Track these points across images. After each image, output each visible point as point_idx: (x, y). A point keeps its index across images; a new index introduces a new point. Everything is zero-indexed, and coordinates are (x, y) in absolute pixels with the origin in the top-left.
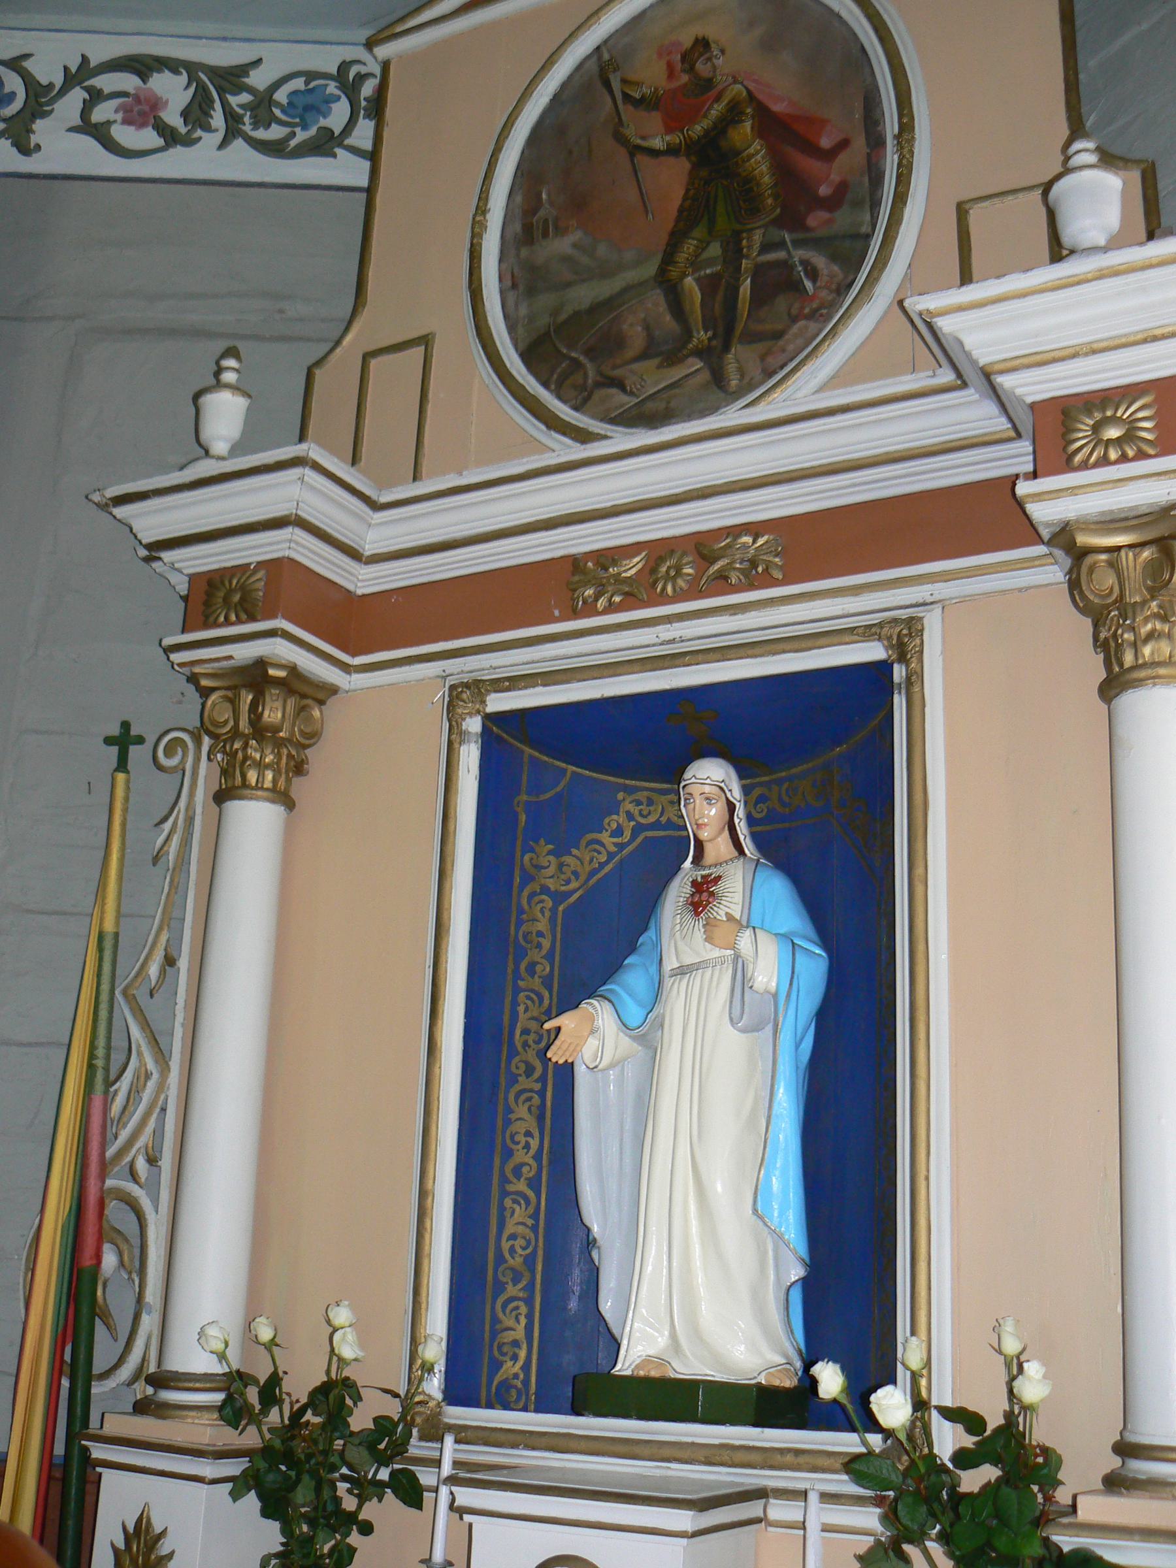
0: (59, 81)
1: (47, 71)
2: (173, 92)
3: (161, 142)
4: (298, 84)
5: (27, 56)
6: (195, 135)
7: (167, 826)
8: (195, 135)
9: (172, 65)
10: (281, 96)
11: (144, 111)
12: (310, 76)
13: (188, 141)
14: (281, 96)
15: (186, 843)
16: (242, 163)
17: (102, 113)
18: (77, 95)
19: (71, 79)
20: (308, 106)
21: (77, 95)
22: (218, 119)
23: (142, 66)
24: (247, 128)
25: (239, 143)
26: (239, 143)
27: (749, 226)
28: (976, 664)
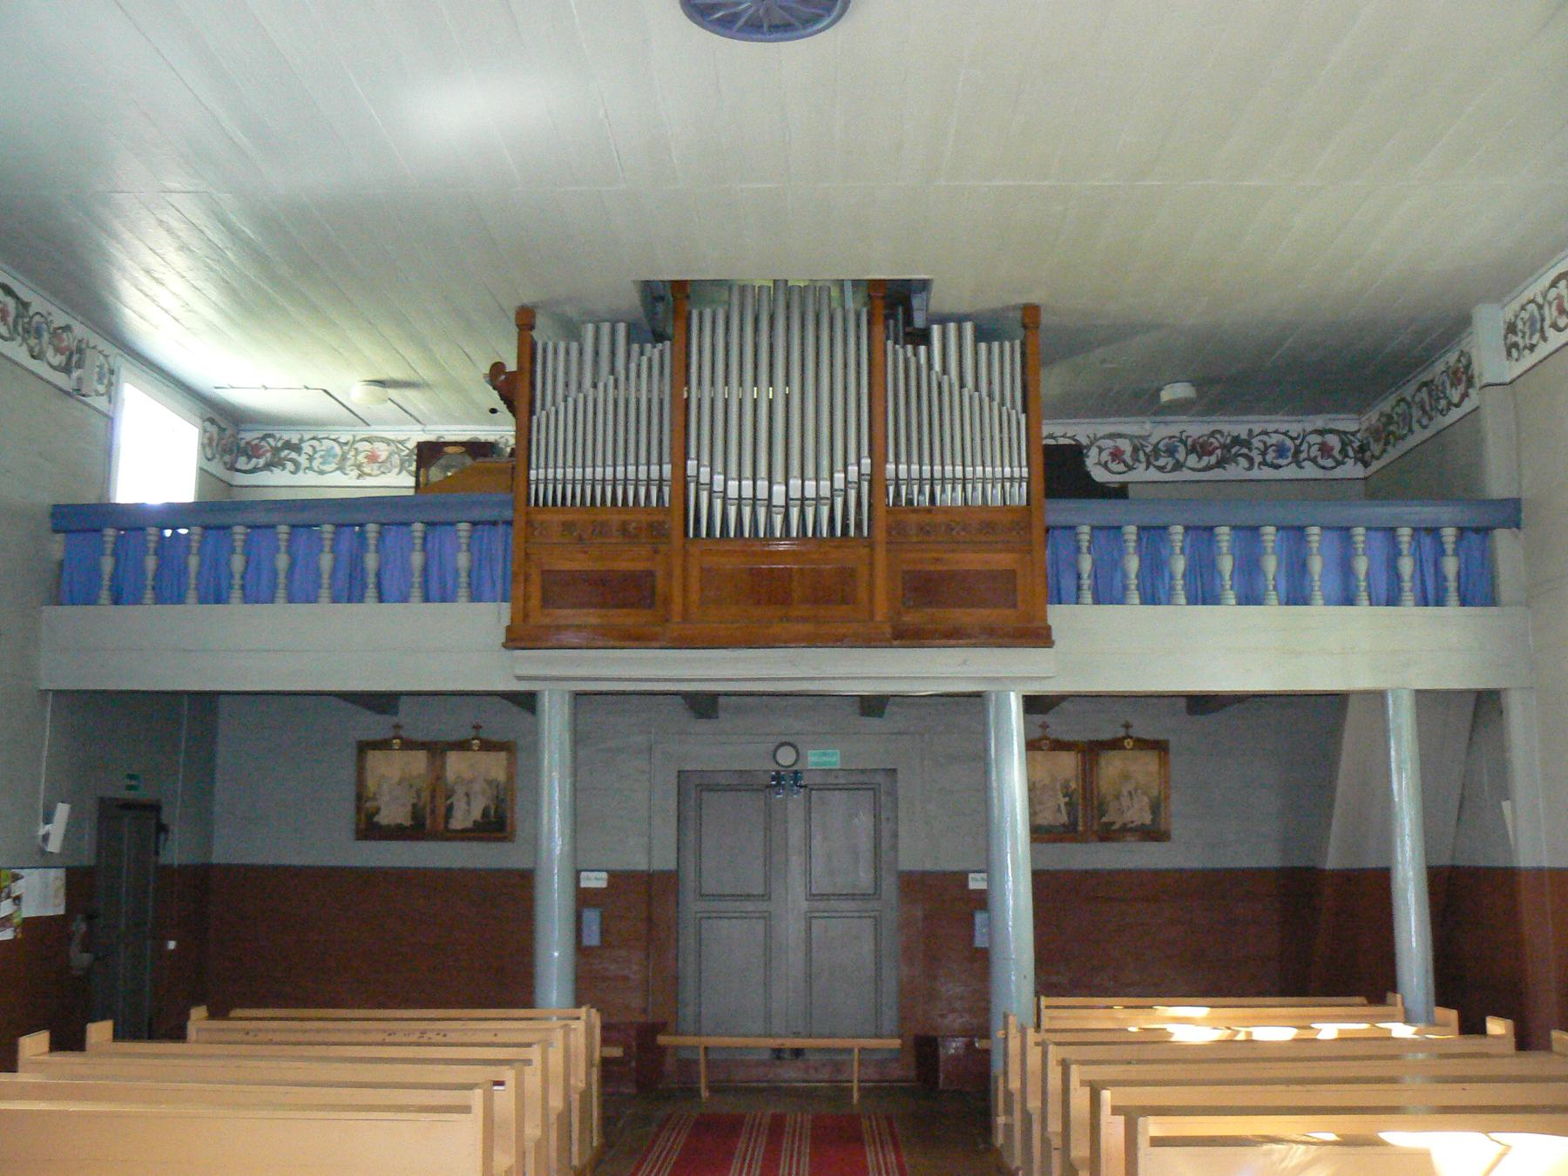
22: (1142, 457)
23: (1321, 432)
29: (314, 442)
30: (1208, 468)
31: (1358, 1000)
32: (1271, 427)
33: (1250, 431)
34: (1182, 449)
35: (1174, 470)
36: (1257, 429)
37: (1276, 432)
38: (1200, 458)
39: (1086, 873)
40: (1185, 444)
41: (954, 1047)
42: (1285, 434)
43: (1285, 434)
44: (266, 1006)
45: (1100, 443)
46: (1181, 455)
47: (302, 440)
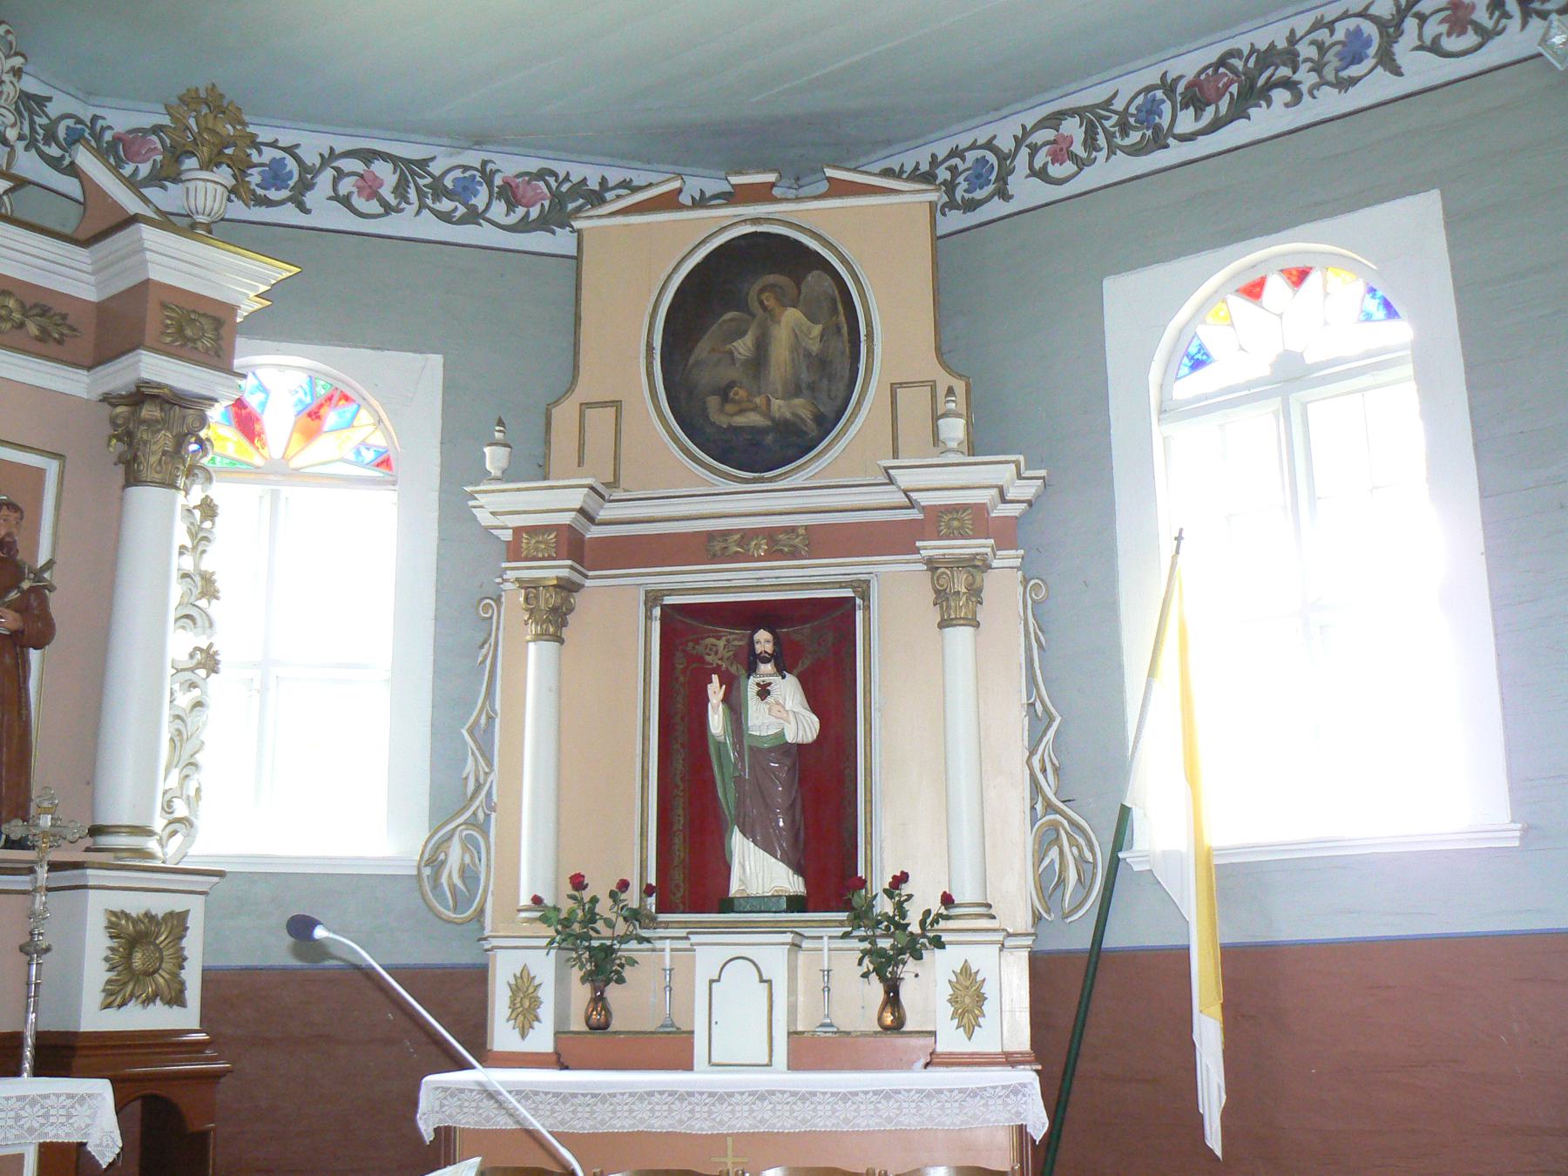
0: (1012, 145)
1: (312, 159)
2: (1073, 129)
3: (382, 210)
4: (458, 173)
5: (297, 146)
6: (1501, 26)
7: (484, 651)
8: (1501, 26)
9: (386, 157)
10: (1132, 110)
11: (370, 188)
12: (466, 168)
13: (399, 210)
14: (1132, 110)
15: (494, 664)
16: (429, 227)
17: (346, 186)
18: (329, 173)
19: (1019, 142)
20: (462, 192)
21: (329, 173)
22: (412, 194)
23: (368, 156)
24: (429, 202)
25: (426, 212)
26: (426, 212)
27: (645, 933)
28: (895, 597)
29: (1322, 35)
30: (524, 226)
31: (1224, 1097)
32: (964, 141)
33: (934, 156)
34: (483, 191)
35: (462, 221)
36: (942, 150)
37: (274, 145)
38: (511, 207)
39: (1059, 952)
40: (490, 184)
41: (494, 459)
42: (290, 150)
43: (290, 150)
44: (713, 777)
45: (340, 163)
46: (480, 201)
47: (1292, 39)
